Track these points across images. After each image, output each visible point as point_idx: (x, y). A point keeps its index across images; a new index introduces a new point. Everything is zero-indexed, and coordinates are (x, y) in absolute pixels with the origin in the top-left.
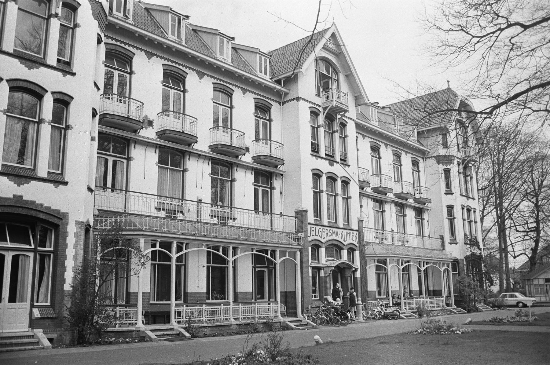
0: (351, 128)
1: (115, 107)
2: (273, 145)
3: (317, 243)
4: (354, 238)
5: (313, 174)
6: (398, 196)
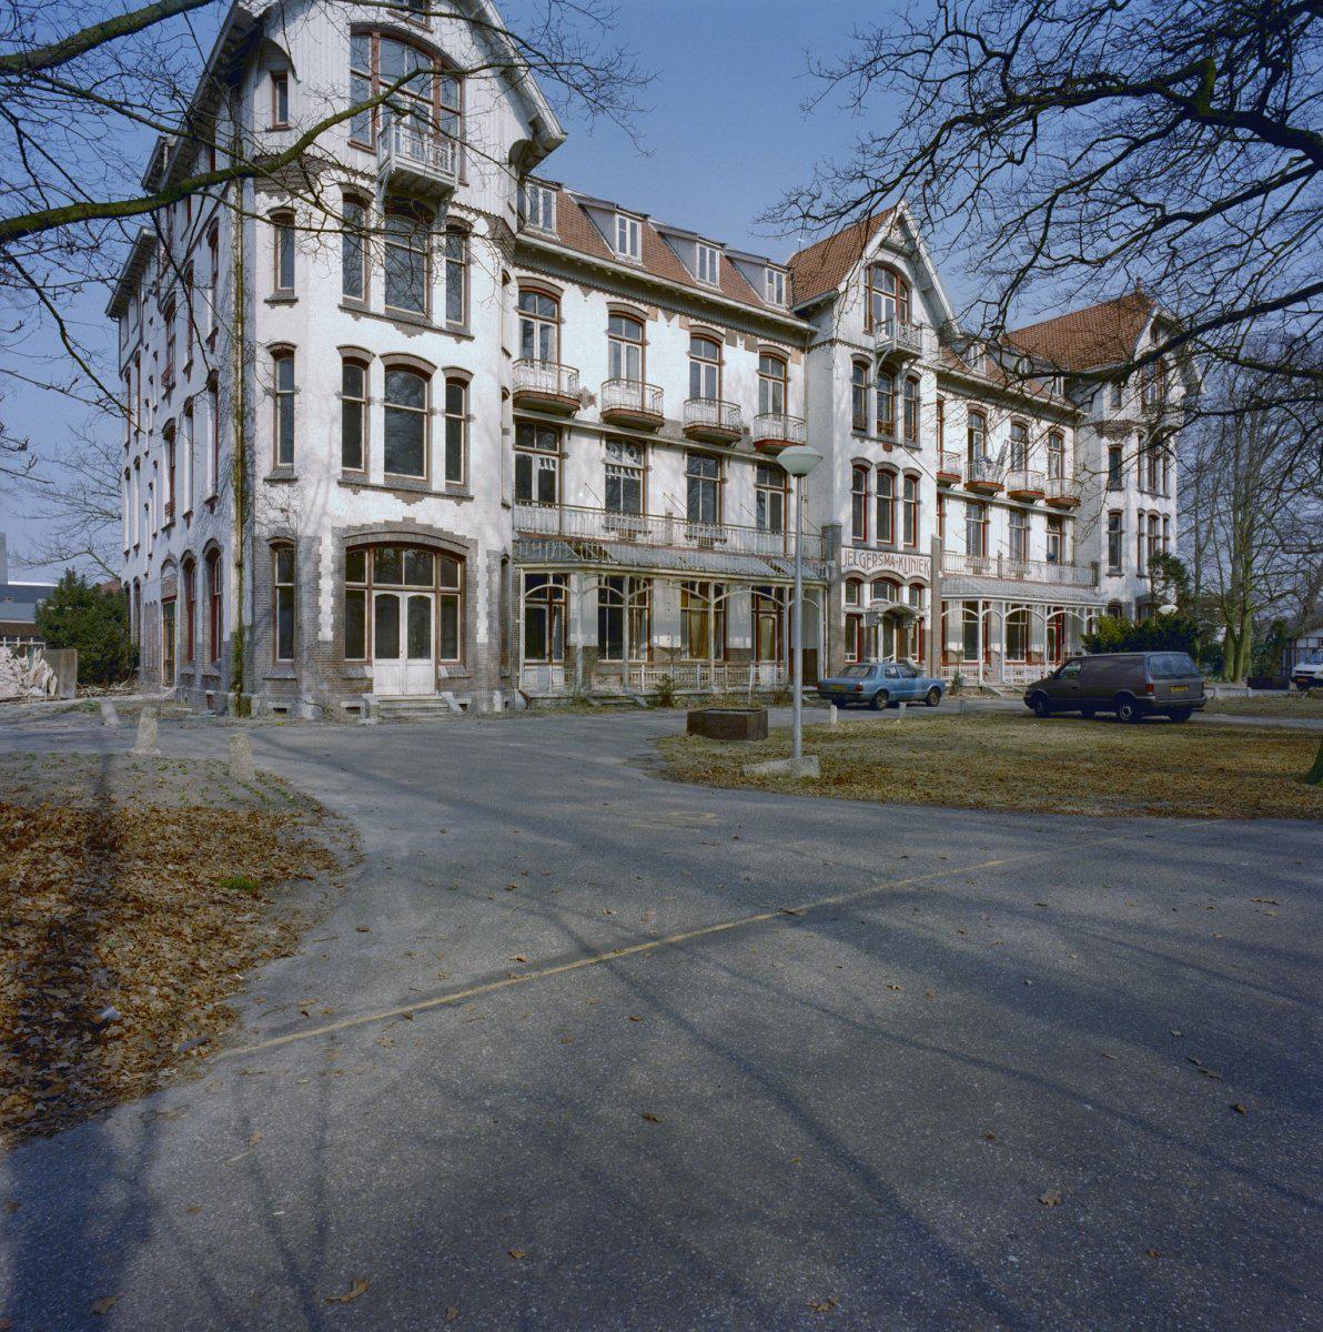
0: (928, 388)
1: (541, 381)
2: (647, 392)
3: (856, 576)
4: (922, 568)
5: (854, 467)
6: (1014, 495)
